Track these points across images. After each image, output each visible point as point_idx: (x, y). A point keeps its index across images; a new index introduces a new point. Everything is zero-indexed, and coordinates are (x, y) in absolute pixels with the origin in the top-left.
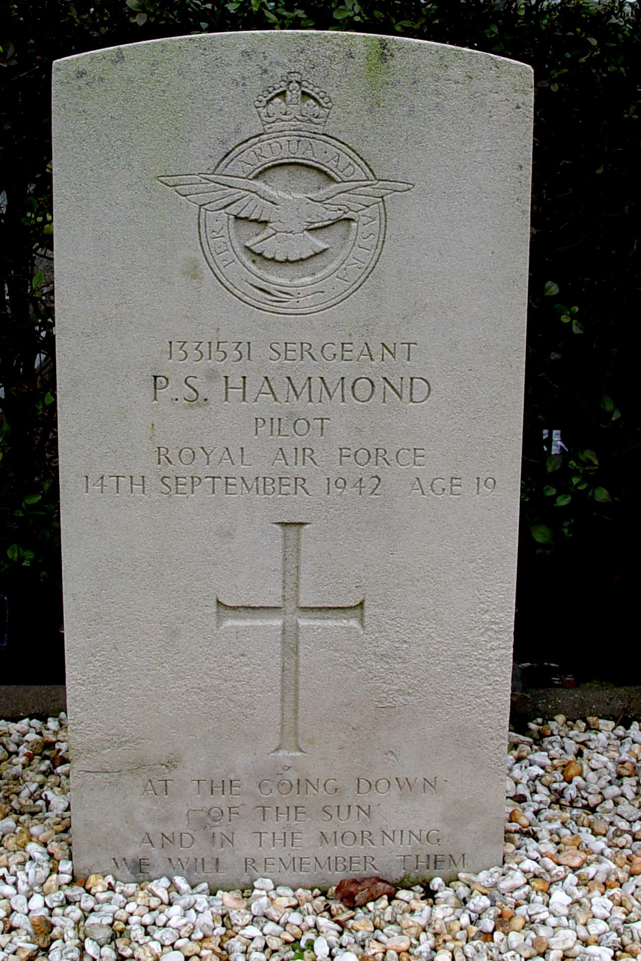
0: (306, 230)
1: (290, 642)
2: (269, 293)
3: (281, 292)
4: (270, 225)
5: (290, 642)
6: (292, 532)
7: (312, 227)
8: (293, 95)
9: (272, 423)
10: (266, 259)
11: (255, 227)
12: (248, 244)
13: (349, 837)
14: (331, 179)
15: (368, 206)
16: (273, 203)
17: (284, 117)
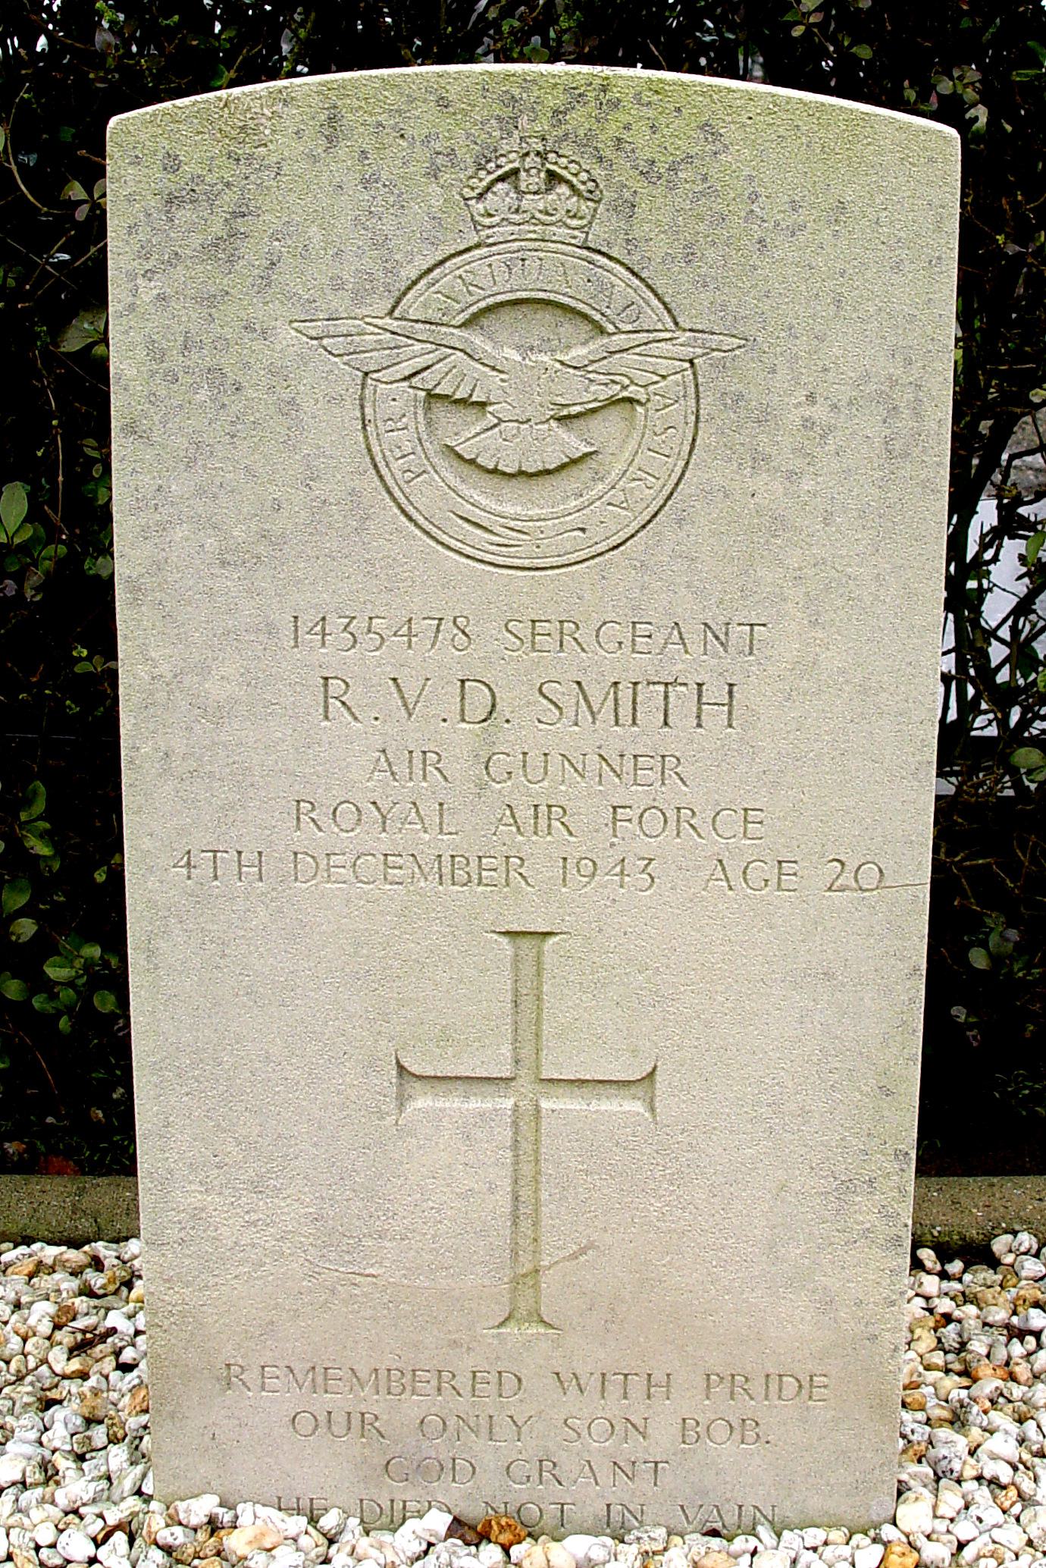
1: (526, 1125)
2: (485, 529)
4: (490, 409)
5: (526, 1125)
6: (525, 943)
7: (565, 412)
8: (532, 180)
9: (411, 758)
11: (474, 411)
15: (664, 377)
17: (569, 221)
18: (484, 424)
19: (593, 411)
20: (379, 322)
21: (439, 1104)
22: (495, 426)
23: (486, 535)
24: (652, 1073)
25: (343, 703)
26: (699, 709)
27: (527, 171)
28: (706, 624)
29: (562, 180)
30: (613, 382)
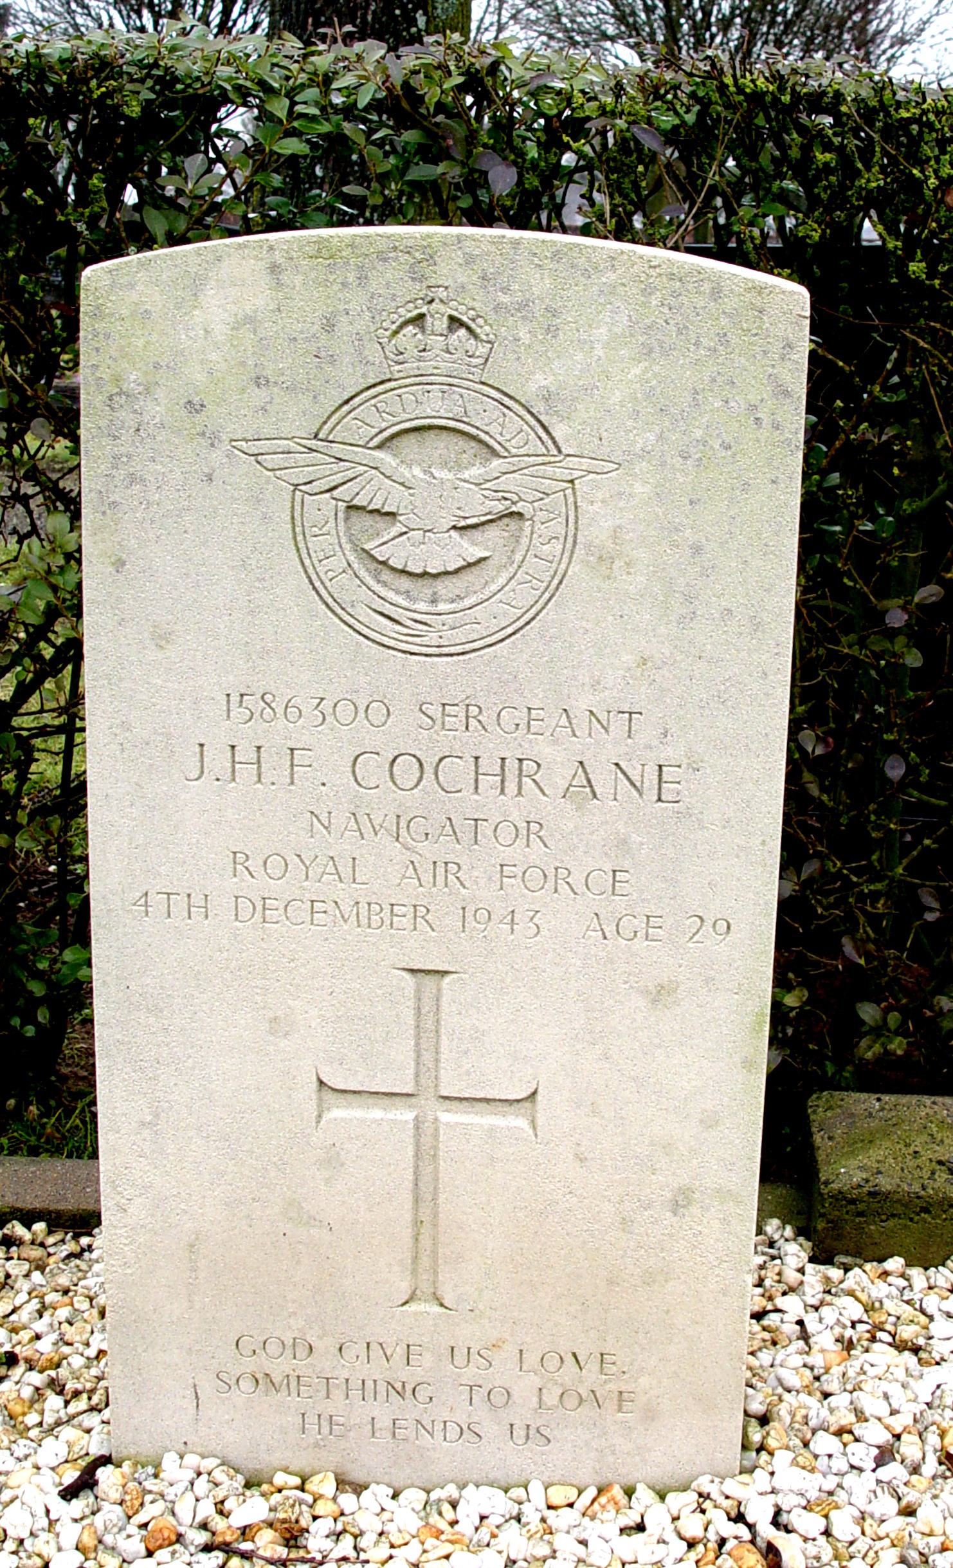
0: (454, 527)
1: (425, 1148)
3: (416, 621)
4: (401, 518)
5: (425, 1148)
6: (429, 982)
7: (462, 523)
10: (393, 569)
11: (381, 523)
12: (366, 547)
13: (273, 1348)
14: (495, 453)
16: (402, 484)
18: (394, 531)
19: (491, 521)
20: (303, 442)
21: (390, 1116)
22: (405, 533)
23: (398, 628)
24: (535, 1093)
25: (534, 780)
26: (233, 767)
27: (432, 316)
28: (591, 712)
29: (462, 324)
30: (506, 499)
